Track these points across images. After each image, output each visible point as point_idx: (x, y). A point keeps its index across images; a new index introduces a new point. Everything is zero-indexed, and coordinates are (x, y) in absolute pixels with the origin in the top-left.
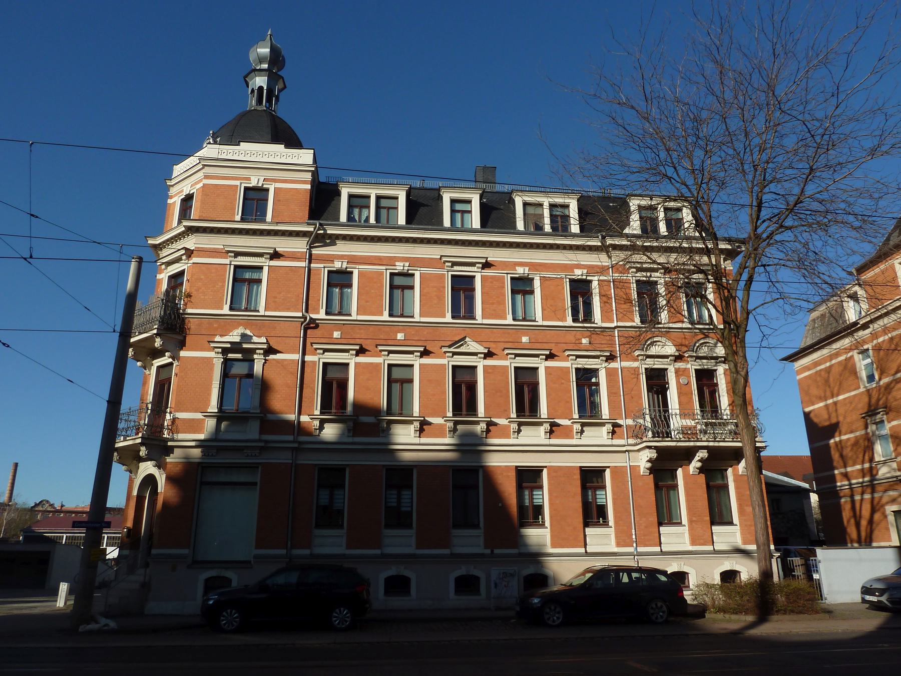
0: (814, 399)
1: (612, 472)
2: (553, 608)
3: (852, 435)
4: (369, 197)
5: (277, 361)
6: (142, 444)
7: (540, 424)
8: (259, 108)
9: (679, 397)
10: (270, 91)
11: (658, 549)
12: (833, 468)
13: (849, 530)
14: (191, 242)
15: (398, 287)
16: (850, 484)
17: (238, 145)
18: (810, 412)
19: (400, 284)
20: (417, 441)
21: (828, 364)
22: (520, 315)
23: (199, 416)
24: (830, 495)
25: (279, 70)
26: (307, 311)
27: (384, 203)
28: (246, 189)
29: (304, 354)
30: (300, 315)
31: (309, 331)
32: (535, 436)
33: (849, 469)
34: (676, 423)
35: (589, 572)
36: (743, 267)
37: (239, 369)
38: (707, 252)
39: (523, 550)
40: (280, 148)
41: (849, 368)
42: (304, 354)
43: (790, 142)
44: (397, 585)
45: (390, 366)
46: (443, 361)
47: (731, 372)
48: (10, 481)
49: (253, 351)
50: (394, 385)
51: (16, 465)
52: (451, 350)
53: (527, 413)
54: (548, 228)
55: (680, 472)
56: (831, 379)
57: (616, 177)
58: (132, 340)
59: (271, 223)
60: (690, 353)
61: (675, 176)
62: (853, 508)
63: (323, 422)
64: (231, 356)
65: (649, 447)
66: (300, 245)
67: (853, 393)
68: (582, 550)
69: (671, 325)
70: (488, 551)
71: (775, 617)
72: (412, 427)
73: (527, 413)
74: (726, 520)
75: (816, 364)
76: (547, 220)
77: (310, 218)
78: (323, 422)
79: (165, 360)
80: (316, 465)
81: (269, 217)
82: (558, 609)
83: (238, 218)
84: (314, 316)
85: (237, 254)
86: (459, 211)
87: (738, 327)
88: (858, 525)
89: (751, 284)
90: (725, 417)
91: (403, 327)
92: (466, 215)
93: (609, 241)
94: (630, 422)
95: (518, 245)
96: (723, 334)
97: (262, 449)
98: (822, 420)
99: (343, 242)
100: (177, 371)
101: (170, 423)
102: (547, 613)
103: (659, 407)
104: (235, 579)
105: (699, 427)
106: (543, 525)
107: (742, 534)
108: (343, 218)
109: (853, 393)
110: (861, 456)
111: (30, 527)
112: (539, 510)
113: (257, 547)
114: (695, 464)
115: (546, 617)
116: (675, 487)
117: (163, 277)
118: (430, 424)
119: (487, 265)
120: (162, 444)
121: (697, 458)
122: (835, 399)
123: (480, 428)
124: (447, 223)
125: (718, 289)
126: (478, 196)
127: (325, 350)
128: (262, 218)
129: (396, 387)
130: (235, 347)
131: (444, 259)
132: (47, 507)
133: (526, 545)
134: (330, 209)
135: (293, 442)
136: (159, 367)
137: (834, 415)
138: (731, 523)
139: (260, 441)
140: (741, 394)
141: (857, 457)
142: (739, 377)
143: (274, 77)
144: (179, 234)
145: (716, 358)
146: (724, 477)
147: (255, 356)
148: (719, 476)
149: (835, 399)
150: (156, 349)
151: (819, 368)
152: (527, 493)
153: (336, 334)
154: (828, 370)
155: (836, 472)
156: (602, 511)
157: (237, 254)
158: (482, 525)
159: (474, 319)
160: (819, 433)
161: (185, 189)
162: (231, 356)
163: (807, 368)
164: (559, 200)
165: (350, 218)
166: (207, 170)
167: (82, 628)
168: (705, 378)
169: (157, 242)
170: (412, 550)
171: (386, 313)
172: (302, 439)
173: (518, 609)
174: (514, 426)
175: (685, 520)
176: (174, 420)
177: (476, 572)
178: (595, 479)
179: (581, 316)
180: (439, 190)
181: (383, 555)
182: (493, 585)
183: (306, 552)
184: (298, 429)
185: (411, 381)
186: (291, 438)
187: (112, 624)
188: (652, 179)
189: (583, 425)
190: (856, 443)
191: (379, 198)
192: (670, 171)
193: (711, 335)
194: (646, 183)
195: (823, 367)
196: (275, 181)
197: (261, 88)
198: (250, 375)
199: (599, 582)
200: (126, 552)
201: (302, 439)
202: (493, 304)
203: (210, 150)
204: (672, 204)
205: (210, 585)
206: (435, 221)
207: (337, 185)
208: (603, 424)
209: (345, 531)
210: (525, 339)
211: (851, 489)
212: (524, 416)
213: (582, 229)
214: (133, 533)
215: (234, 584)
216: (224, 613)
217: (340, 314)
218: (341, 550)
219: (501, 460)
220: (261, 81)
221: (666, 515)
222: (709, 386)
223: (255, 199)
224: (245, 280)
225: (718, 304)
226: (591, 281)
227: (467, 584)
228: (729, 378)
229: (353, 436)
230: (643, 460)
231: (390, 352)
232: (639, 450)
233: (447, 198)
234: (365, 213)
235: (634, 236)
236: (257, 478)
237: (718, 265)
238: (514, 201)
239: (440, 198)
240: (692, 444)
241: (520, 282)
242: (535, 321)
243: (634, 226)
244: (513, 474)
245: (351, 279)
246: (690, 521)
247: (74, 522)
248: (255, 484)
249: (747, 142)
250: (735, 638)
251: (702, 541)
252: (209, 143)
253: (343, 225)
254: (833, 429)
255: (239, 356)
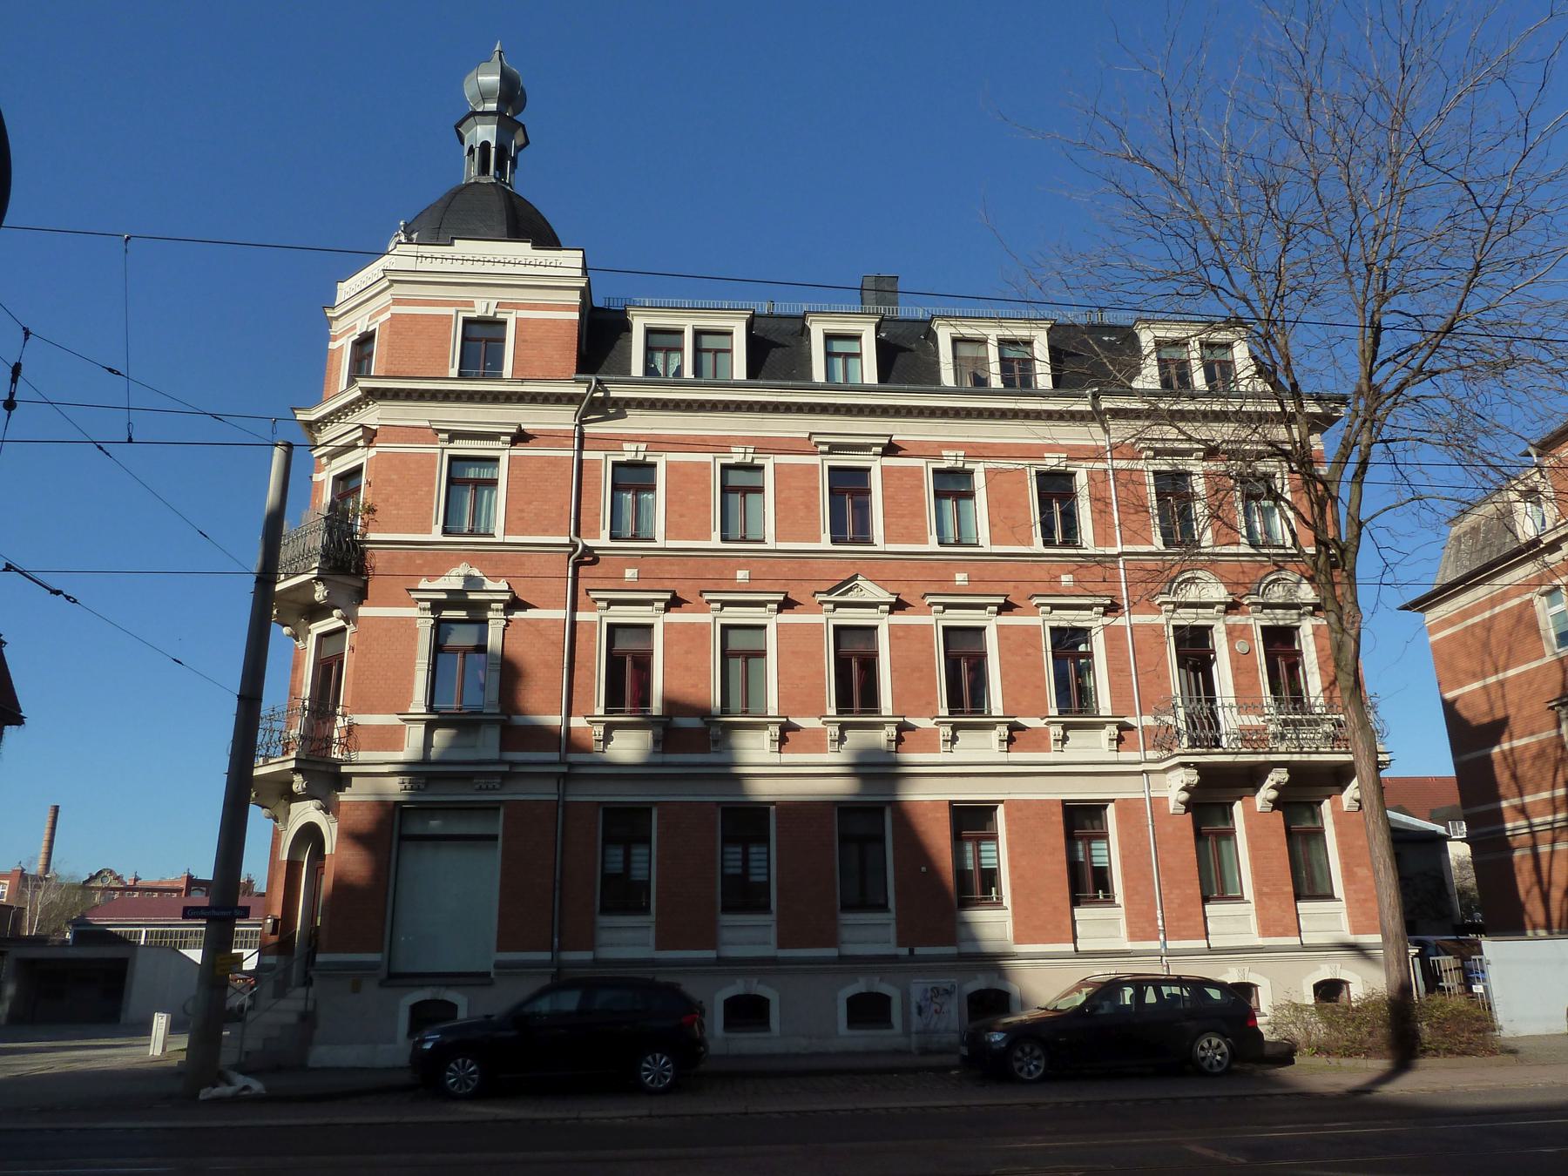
0: (1461, 676)
1: (1119, 812)
2: (1027, 1050)
3: (1533, 739)
4: (681, 332)
5: (522, 619)
6: (296, 770)
7: (990, 726)
8: (484, 180)
9: (1235, 676)
10: (502, 150)
11: (1202, 944)
12: (1499, 798)
13: (1529, 907)
14: (373, 415)
15: (736, 490)
16: (1531, 826)
17: (451, 244)
18: (1455, 700)
19: (739, 484)
20: (776, 758)
21: (1487, 614)
22: (951, 535)
23: (393, 720)
24: (1491, 846)
25: (518, 111)
26: (578, 534)
27: (707, 342)
28: (467, 321)
29: (574, 609)
30: (566, 540)
31: (582, 569)
32: (983, 747)
33: (1528, 799)
34: (1230, 720)
35: (1088, 985)
36: (1347, 446)
37: (461, 637)
38: (1287, 419)
39: (967, 948)
40: (523, 249)
41: (1525, 621)
42: (574, 609)
43: (1433, 221)
44: (748, 1012)
45: (725, 628)
46: (819, 619)
47: (1332, 630)
48: (46, 837)
49: (486, 605)
50: (732, 661)
51: (56, 809)
52: (833, 598)
53: (967, 708)
54: (996, 382)
55: (1238, 808)
56: (1493, 641)
57: (1124, 288)
58: (279, 587)
59: (512, 380)
60: (1254, 599)
61: (1226, 284)
62: (1537, 867)
63: (610, 728)
64: (446, 614)
65: (1185, 765)
66: (563, 419)
67: (1534, 665)
68: (1070, 947)
69: (1217, 550)
70: (904, 951)
71: (1423, 1062)
72: (766, 733)
73: (967, 708)
74: (1320, 892)
75: (1465, 614)
76: (995, 368)
77: (578, 372)
78: (610, 728)
79: (333, 622)
80: (718, 803)
81: (507, 371)
82: (1037, 1053)
83: (454, 372)
84: (590, 543)
85: (454, 436)
86: (839, 355)
87: (1343, 551)
88: (1545, 898)
89: (1364, 473)
90: (1318, 710)
91: (747, 560)
92: (851, 361)
93: (1105, 404)
94: (1148, 720)
95: (944, 413)
96: (1315, 563)
97: (505, 777)
98: (1477, 714)
99: (638, 412)
100: (354, 643)
101: (344, 733)
102: (1019, 1060)
103: (1198, 693)
104: (465, 1006)
105: (1272, 728)
106: (998, 904)
107: (1350, 915)
108: (637, 369)
109: (1534, 665)
110: (1550, 775)
111: (83, 916)
112: (990, 878)
113: (500, 949)
114: (1266, 793)
115: (1017, 1065)
116: (1230, 834)
117: (325, 478)
118: (797, 728)
119: (891, 449)
120: (331, 770)
121: (1269, 783)
122: (1501, 676)
123: (883, 737)
124: (819, 375)
125: (1306, 483)
126: (872, 328)
127: (611, 603)
128: (494, 372)
129: (737, 665)
130: (455, 599)
131: (816, 439)
132: (110, 881)
133: (974, 939)
134: (613, 354)
135: (560, 763)
136: (321, 637)
137: (1499, 704)
138: (1330, 896)
139: (501, 762)
140: (1350, 669)
141: (1543, 778)
142: (1346, 638)
143: (507, 125)
144: (352, 403)
145: (1296, 606)
146: (1316, 816)
147: (490, 615)
148: (1308, 814)
149: (1501, 676)
150: (317, 603)
151: (1470, 622)
152: (969, 847)
153: (630, 573)
154: (1488, 625)
155: (1504, 804)
156: (1101, 878)
157: (454, 436)
158: (892, 904)
159: (871, 543)
160: (1471, 737)
161: (358, 323)
162: (446, 614)
163: (1449, 622)
164: (1019, 332)
165: (649, 369)
166: (398, 290)
167: (205, 1093)
168: (1280, 641)
169: (313, 418)
170: (771, 950)
171: (716, 535)
172: (573, 757)
173: (964, 1051)
174: (946, 731)
175: (1249, 893)
176: (350, 729)
177: (884, 988)
178: (1087, 823)
179: (1058, 537)
180: (803, 318)
181: (720, 961)
182: (914, 1010)
183: (587, 956)
184: (565, 742)
185: (762, 654)
186: (555, 756)
187: (257, 1086)
188: (1187, 290)
189: (1067, 727)
190: (1541, 754)
191: (698, 334)
192: (1217, 276)
193: (1288, 566)
194: (1176, 298)
195: (1477, 619)
196: (517, 306)
197: (485, 146)
198: (481, 648)
199: (1106, 1004)
200: (271, 960)
201: (573, 757)
202: (903, 516)
203: (402, 256)
204: (1219, 337)
205: (423, 1016)
206: (797, 372)
207: (625, 312)
208: (1101, 726)
209: (653, 918)
210: (961, 577)
211: (1533, 833)
212: (962, 713)
213: (1057, 381)
214: (284, 925)
215: (462, 1014)
216: (452, 1065)
217: (635, 538)
218: (648, 952)
219: (927, 795)
220: (485, 132)
221: (1214, 885)
222: (1286, 656)
223: (482, 339)
224: (467, 482)
225: (1304, 507)
226: (971, 472)
227: (869, 1010)
228: (1327, 644)
229: (663, 752)
230: (1174, 787)
231: (725, 604)
232: (1165, 771)
233: (944, 335)
234: (675, 360)
235: (1152, 393)
236: (499, 829)
237: (1304, 443)
238: (935, 334)
239: (805, 332)
240: (1262, 758)
241: (950, 477)
242: (977, 545)
243: (1149, 377)
244: (1058, 818)
245: (653, 477)
246: (1259, 894)
247: (186, 909)
248: (495, 838)
249: (1355, 226)
250: (1355, 1102)
251: (1280, 930)
252: (400, 242)
253: (637, 382)
254: (1497, 729)
255: (462, 614)
